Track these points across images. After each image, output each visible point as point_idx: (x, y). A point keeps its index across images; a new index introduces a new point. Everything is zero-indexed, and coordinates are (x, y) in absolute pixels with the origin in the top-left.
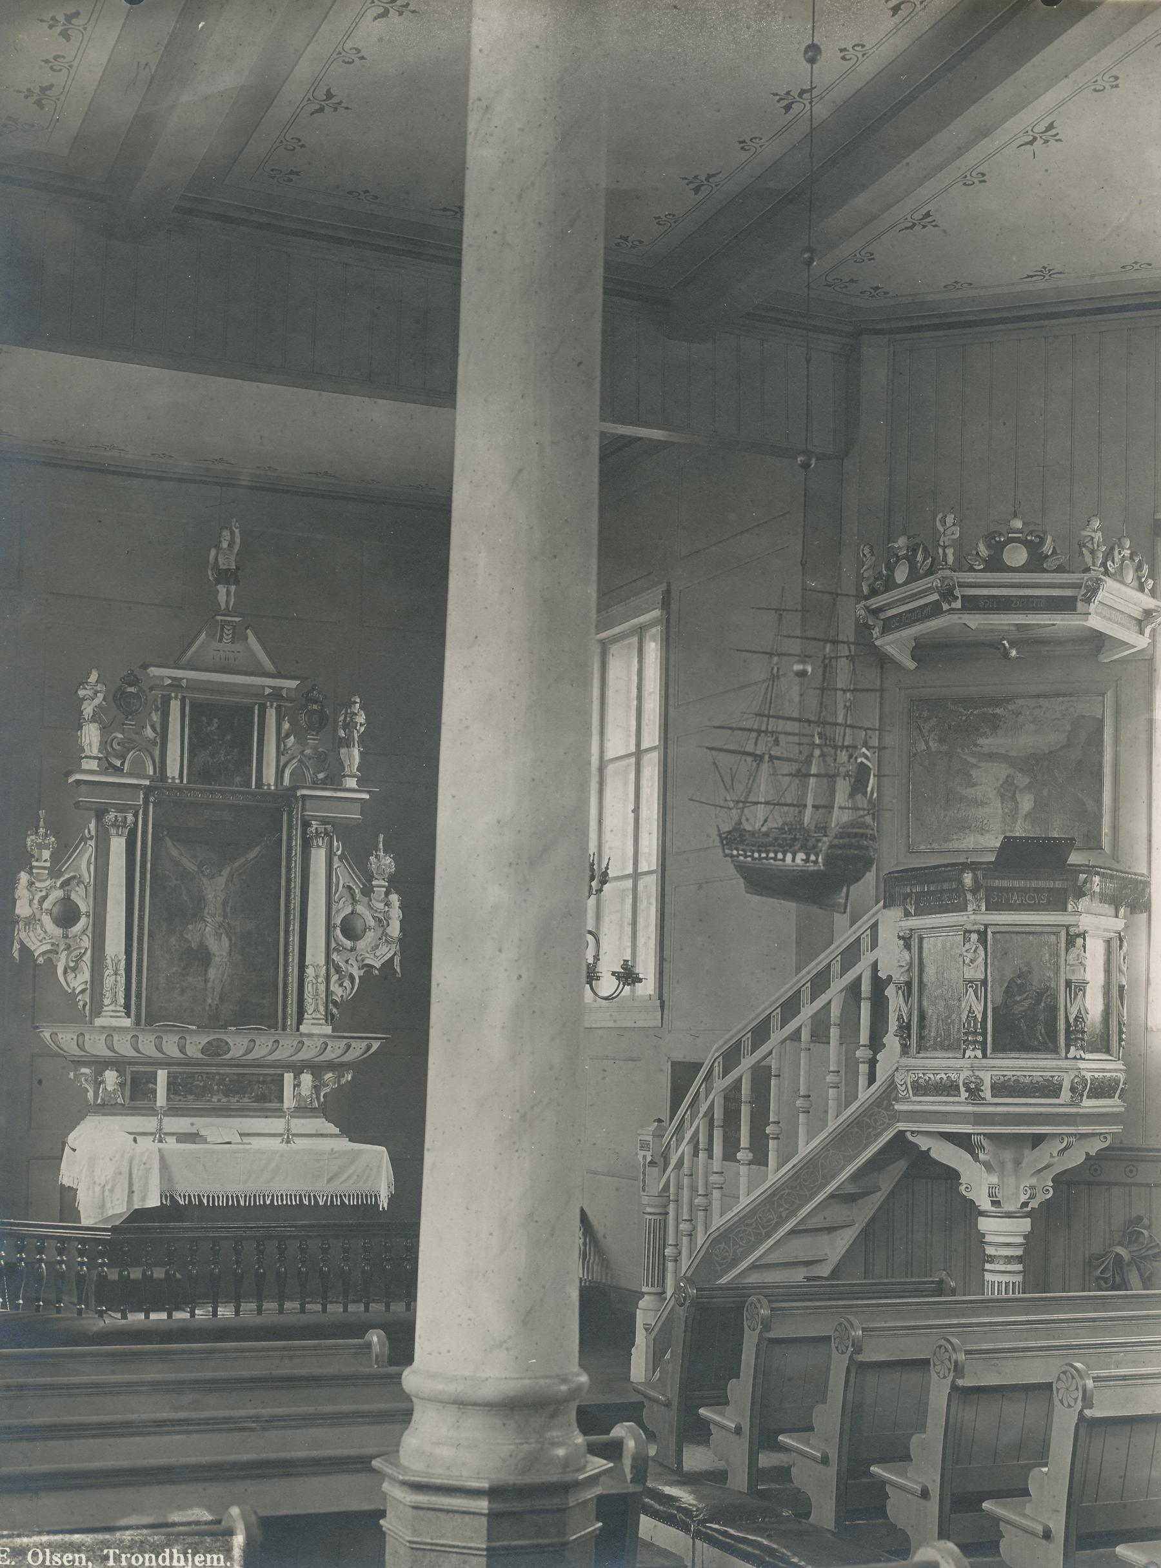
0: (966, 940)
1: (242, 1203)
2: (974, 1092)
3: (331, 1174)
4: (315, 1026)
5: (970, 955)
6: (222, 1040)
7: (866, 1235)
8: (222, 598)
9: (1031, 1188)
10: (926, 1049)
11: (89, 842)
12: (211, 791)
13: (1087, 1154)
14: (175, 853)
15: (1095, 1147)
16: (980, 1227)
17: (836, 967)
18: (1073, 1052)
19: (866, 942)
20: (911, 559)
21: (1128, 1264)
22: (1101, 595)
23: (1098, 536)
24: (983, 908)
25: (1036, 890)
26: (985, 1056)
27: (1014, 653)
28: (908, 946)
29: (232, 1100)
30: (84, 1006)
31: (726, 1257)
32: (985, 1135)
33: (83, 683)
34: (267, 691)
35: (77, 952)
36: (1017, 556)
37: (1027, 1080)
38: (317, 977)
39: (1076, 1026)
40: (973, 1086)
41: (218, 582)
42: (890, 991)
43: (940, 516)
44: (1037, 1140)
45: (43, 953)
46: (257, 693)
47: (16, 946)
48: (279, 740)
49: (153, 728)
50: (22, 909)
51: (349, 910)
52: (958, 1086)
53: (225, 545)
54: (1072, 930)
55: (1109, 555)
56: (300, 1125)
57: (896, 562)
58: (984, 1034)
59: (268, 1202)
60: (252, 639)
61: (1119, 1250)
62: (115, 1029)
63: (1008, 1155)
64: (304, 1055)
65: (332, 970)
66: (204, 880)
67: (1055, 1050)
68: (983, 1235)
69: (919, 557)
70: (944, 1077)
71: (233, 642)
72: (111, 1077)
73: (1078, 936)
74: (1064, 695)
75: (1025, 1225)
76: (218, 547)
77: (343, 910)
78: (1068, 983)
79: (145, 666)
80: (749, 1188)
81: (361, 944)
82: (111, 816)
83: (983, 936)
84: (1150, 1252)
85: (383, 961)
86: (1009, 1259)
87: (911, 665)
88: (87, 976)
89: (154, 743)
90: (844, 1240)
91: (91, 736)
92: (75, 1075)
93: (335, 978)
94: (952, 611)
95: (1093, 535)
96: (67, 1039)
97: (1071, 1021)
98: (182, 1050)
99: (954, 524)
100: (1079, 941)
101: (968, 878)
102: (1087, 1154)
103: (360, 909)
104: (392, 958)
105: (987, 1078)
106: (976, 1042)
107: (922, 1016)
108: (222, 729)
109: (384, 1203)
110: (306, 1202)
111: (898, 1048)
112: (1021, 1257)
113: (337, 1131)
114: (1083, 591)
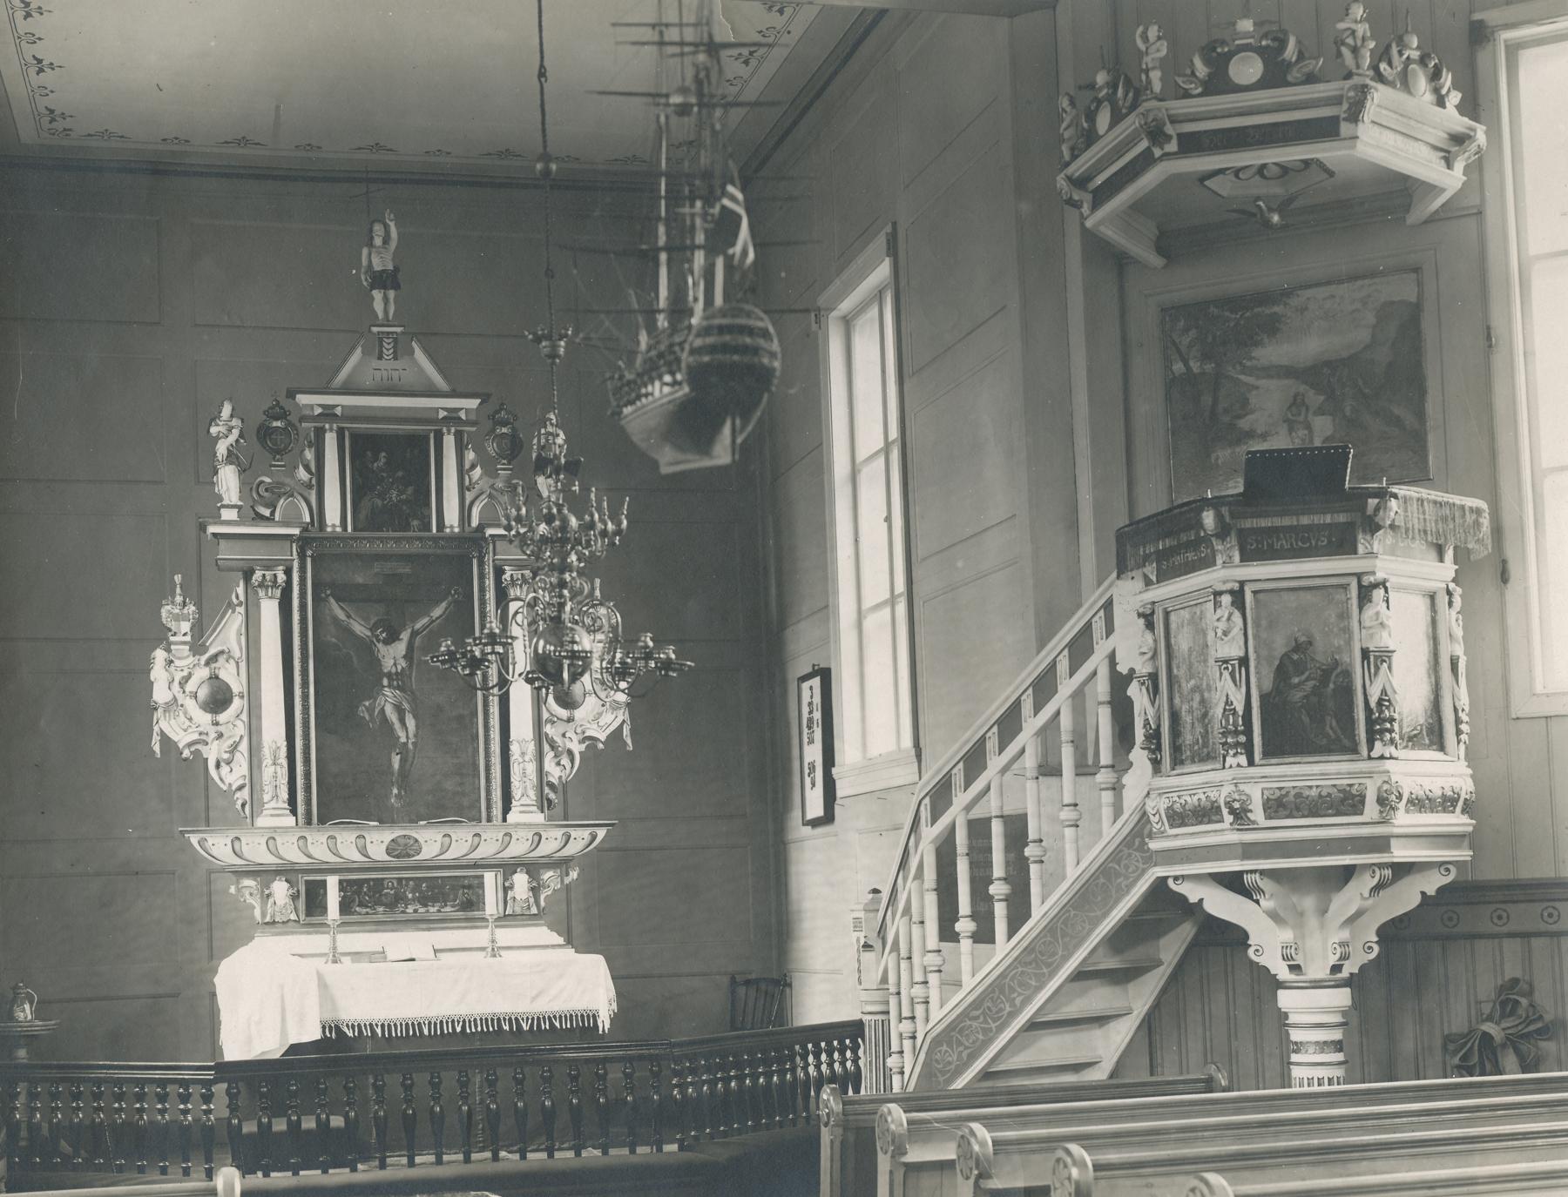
0: (1217, 605)
1: (426, 1032)
2: (1240, 815)
3: (534, 993)
4: (525, 812)
5: (1222, 626)
6: (410, 837)
7: (1149, 1024)
8: (378, 306)
9: (1342, 944)
10: (1182, 763)
11: (238, 609)
12: (381, 539)
13: (1423, 893)
14: (341, 615)
15: (1432, 883)
16: (1280, 1005)
17: (1063, 665)
18: (1379, 748)
19: (1099, 626)
21: (1504, 1046)
22: (1371, 111)
23: (1362, 29)
24: (1237, 558)
25: (1309, 528)
26: (1251, 763)
27: (1276, 218)
28: (1150, 626)
29: (432, 909)
30: (243, 805)
31: (950, 1063)
32: (1262, 872)
33: (214, 419)
34: (442, 414)
35: (231, 742)
36: (1247, 69)
37: (1314, 792)
38: (523, 754)
39: (1381, 712)
40: (1236, 805)
41: (373, 287)
42: (1135, 692)
43: (1141, 29)
44: (1348, 873)
45: (190, 745)
46: (427, 418)
47: (156, 738)
48: (461, 472)
49: (307, 468)
50: (160, 694)
52: (1219, 808)
53: (378, 241)
54: (1366, 580)
55: (1383, 54)
56: (506, 936)
57: (1097, 108)
58: (1248, 732)
59: (458, 1029)
60: (419, 355)
61: (1489, 1028)
62: (275, 829)
63: (1309, 902)
64: (518, 849)
65: (546, 747)
66: (380, 646)
67: (1354, 750)
68: (1286, 1015)
70: (1203, 797)
71: (395, 358)
72: (280, 889)
73: (1375, 586)
74: (1364, 277)
75: (1343, 997)
76: (370, 245)
78: (1365, 653)
79: (291, 394)
80: (977, 966)
81: (579, 714)
82: (258, 575)
83: (1238, 597)
84: (1532, 1028)
85: (608, 731)
86: (1323, 1046)
87: (1157, 261)
88: (245, 770)
89: (310, 486)
90: (1119, 1035)
91: (228, 481)
92: (239, 890)
93: (549, 756)
94: (1167, 156)
95: (1353, 26)
96: (219, 846)
97: (1373, 705)
98: (363, 851)
99: (1159, 38)
100: (1378, 594)
101: (1209, 519)
102: (1423, 893)
104: (621, 727)
105: (1256, 796)
106: (1237, 744)
107: (1175, 717)
108: (391, 465)
109: (604, 1022)
110: (506, 1028)
111: (1149, 766)
112: (1340, 1042)
113: (561, 940)
114: (1345, 106)
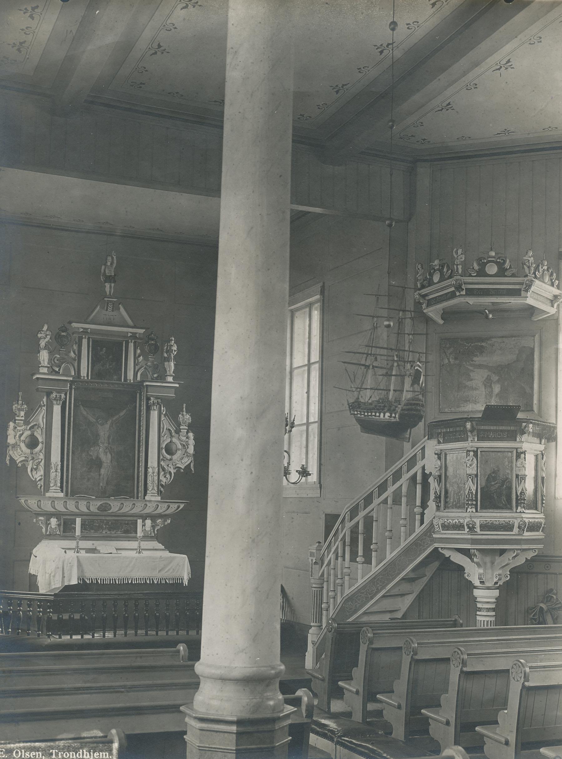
0: (468, 455)
1: (117, 582)
2: (472, 529)
3: (160, 568)
4: (153, 497)
5: (470, 462)
6: (107, 503)
7: (419, 598)
8: (107, 289)
9: (499, 575)
10: (448, 508)
11: (43, 408)
12: (102, 383)
13: (526, 558)
14: (85, 413)
15: (530, 555)
16: (474, 594)
17: (405, 468)
18: (519, 509)
19: (419, 456)
20: (441, 271)
21: (546, 612)
22: (533, 288)
23: (531, 259)
24: (476, 439)
25: (501, 431)
26: (477, 511)
27: (491, 316)
28: (439, 458)
29: (112, 532)
30: (41, 487)
31: (351, 609)
32: (477, 549)
33: (40, 331)
34: (129, 335)
35: (37, 461)
36: (492, 269)
37: (497, 523)
38: (153, 473)
39: (521, 496)
40: (471, 526)
41: (105, 282)
42: (431, 480)
43: (455, 250)
44: (502, 552)
45: (21, 462)
46: (125, 335)
47: (8, 458)
48: (135, 358)
49: (74, 352)
50: (11, 440)
51: (169, 440)
52: (464, 526)
53: (109, 264)
54: (519, 450)
55: (537, 269)
56: (145, 544)
57: (434, 272)
58: (476, 501)
59: (130, 582)
60: (122, 309)
61: (542, 605)
62: (56, 498)
63: (488, 559)
64: (147, 511)
65: (161, 470)
66: (99, 426)
67: (511, 508)
68: (476, 598)
69: (445, 270)
70: (457, 521)
71: (113, 311)
72: (54, 521)
73: (522, 453)
74: (515, 337)
75: (496, 593)
76: (105, 265)
77: (166, 440)
78: (517, 476)
79: (70, 323)
80: (362, 575)
81: (175, 457)
82: (54, 395)
83: (476, 453)
84: (557, 606)
85: (185, 465)
86: (488, 610)
87: (441, 322)
88: (42, 472)
89: (75, 360)
90: (409, 600)
91: (44, 356)
92: (36, 520)
93: (162, 473)
94: (461, 296)
95: (529, 259)
96: (32, 503)
97: (519, 494)
98: (88, 508)
99: (462, 254)
100: (523, 456)
101: (468, 425)
102: (526, 558)
103: (174, 440)
104: (190, 464)
105: (478, 522)
106: (472, 504)
107: (446, 492)
108: (108, 353)
109: (186, 582)
110: (148, 582)
111: (435, 507)
112: (494, 608)
113: (163, 547)
114: (524, 286)
